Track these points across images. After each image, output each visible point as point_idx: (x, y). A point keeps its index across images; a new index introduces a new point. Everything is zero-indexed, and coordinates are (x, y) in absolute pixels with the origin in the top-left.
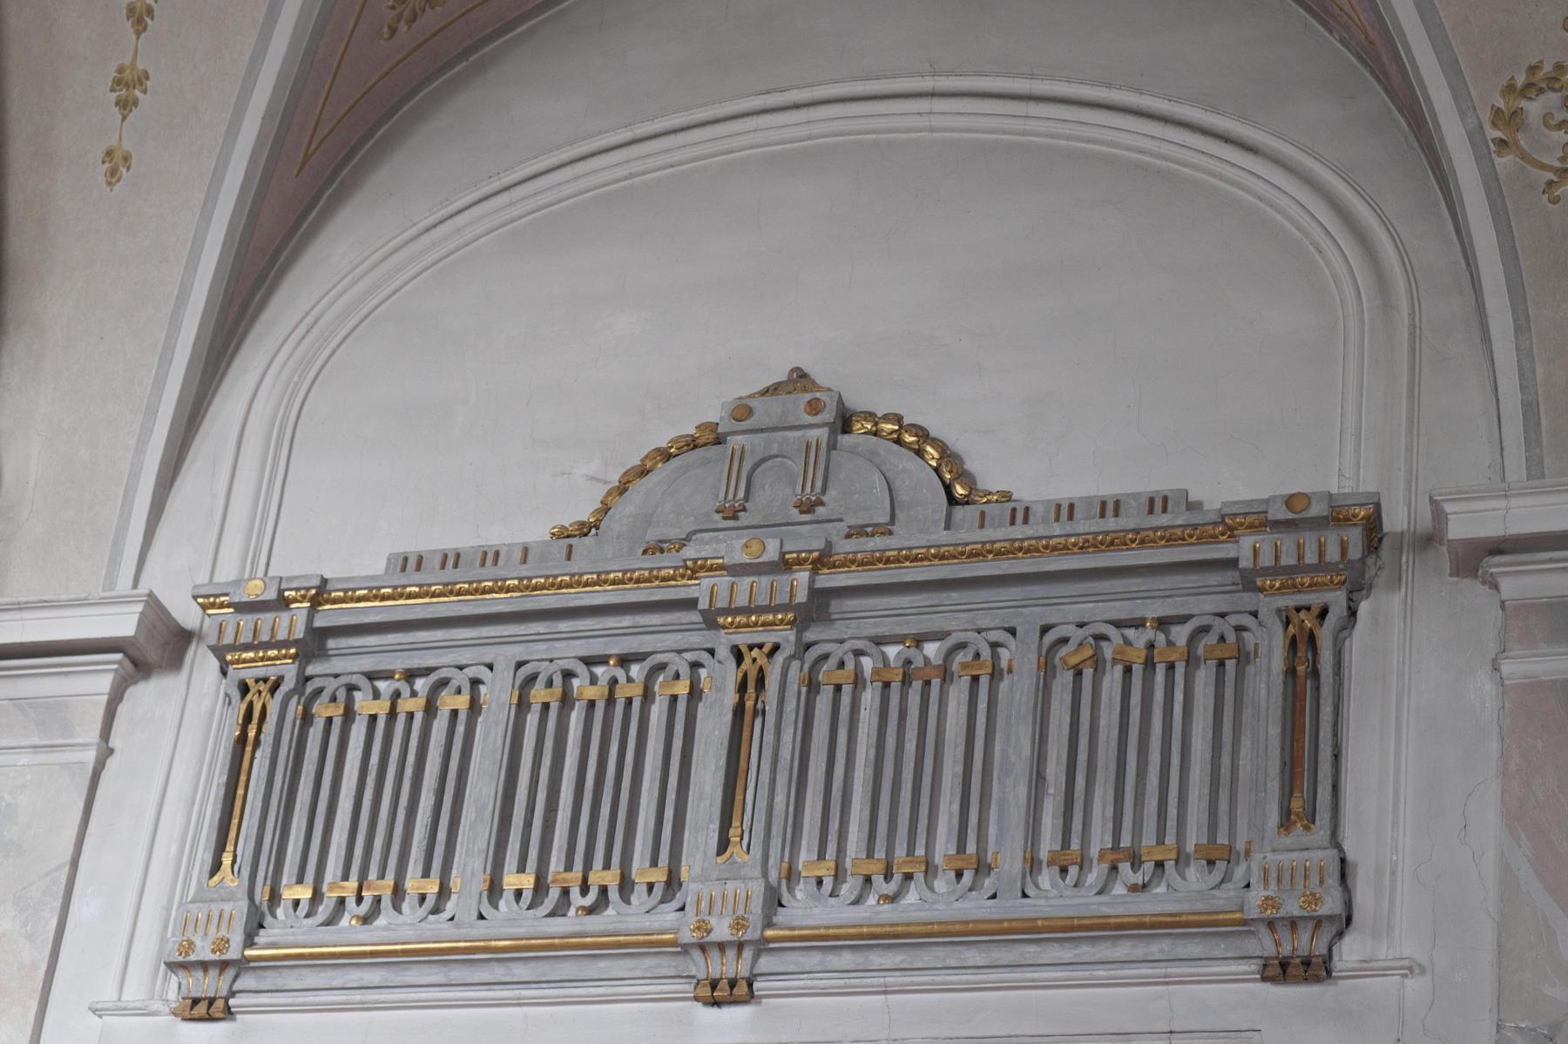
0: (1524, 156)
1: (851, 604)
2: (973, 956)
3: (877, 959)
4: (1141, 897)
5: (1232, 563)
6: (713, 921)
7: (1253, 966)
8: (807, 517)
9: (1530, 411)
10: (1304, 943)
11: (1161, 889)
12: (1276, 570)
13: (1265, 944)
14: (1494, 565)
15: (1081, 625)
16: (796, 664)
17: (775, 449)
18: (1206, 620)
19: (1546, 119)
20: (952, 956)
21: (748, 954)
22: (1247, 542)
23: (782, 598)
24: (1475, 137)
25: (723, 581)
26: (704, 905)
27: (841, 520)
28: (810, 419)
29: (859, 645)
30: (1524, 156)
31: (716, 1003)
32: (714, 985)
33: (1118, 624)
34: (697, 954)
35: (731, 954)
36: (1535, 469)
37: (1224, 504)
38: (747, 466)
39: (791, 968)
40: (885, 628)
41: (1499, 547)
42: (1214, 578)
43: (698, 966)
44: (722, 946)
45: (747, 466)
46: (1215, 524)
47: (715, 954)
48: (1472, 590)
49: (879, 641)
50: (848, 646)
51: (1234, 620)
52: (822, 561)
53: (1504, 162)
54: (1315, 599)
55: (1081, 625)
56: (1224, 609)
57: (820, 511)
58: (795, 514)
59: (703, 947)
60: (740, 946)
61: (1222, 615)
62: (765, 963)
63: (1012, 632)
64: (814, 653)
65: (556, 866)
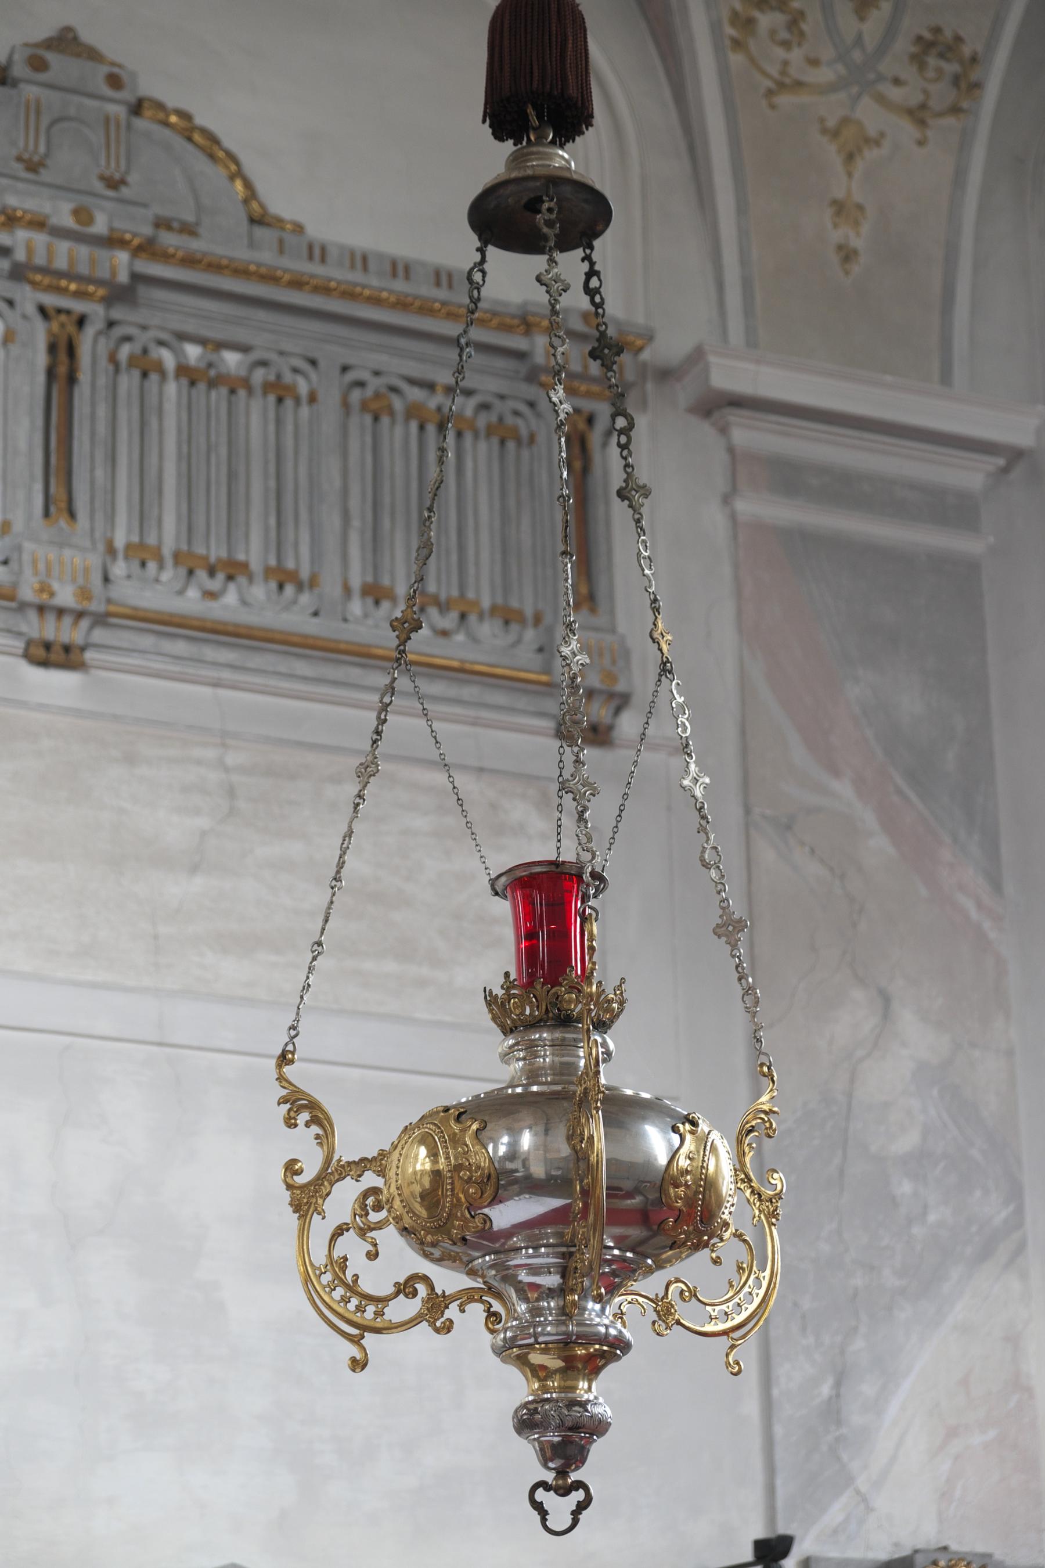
0: (752, 60)
1: (160, 294)
2: (302, 667)
3: (210, 653)
4: (442, 641)
5: (520, 355)
6: (56, 586)
7: (19, 645)
8: (111, 193)
9: (747, 284)
10: (68, 632)
11: (460, 637)
12: (45, 271)
13: (33, 626)
14: (734, 416)
15: (377, 373)
16: (102, 341)
17: (72, 111)
18: (489, 399)
19: (773, 33)
20: (284, 664)
21: (85, 623)
22: (22, 235)
23: (104, 273)
24: (715, 28)
25: (40, 239)
26: (41, 566)
27: (145, 205)
28: (108, 92)
29: (164, 336)
30: (752, 60)
31: (44, 664)
32: (48, 646)
33: (412, 382)
34: (32, 615)
35: (67, 620)
36: (751, 342)
37: (525, 304)
38: (45, 122)
39: (125, 645)
40: (190, 327)
41: (737, 402)
42: (500, 363)
43: (33, 626)
44: (61, 612)
45: (45, 122)
46: (513, 317)
47: (51, 618)
48: (705, 430)
49: (183, 337)
50: (152, 334)
51: (511, 404)
52: (146, 249)
53: (736, 59)
54: (79, 307)
55: (377, 373)
56: (505, 391)
57: (125, 191)
58: (99, 187)
59: (41, 609)
60: (80, 615)
61: (502, 397)
62: (99, 635)
63: (313, 363)
64: (118, 332)
65: (129, 531)
